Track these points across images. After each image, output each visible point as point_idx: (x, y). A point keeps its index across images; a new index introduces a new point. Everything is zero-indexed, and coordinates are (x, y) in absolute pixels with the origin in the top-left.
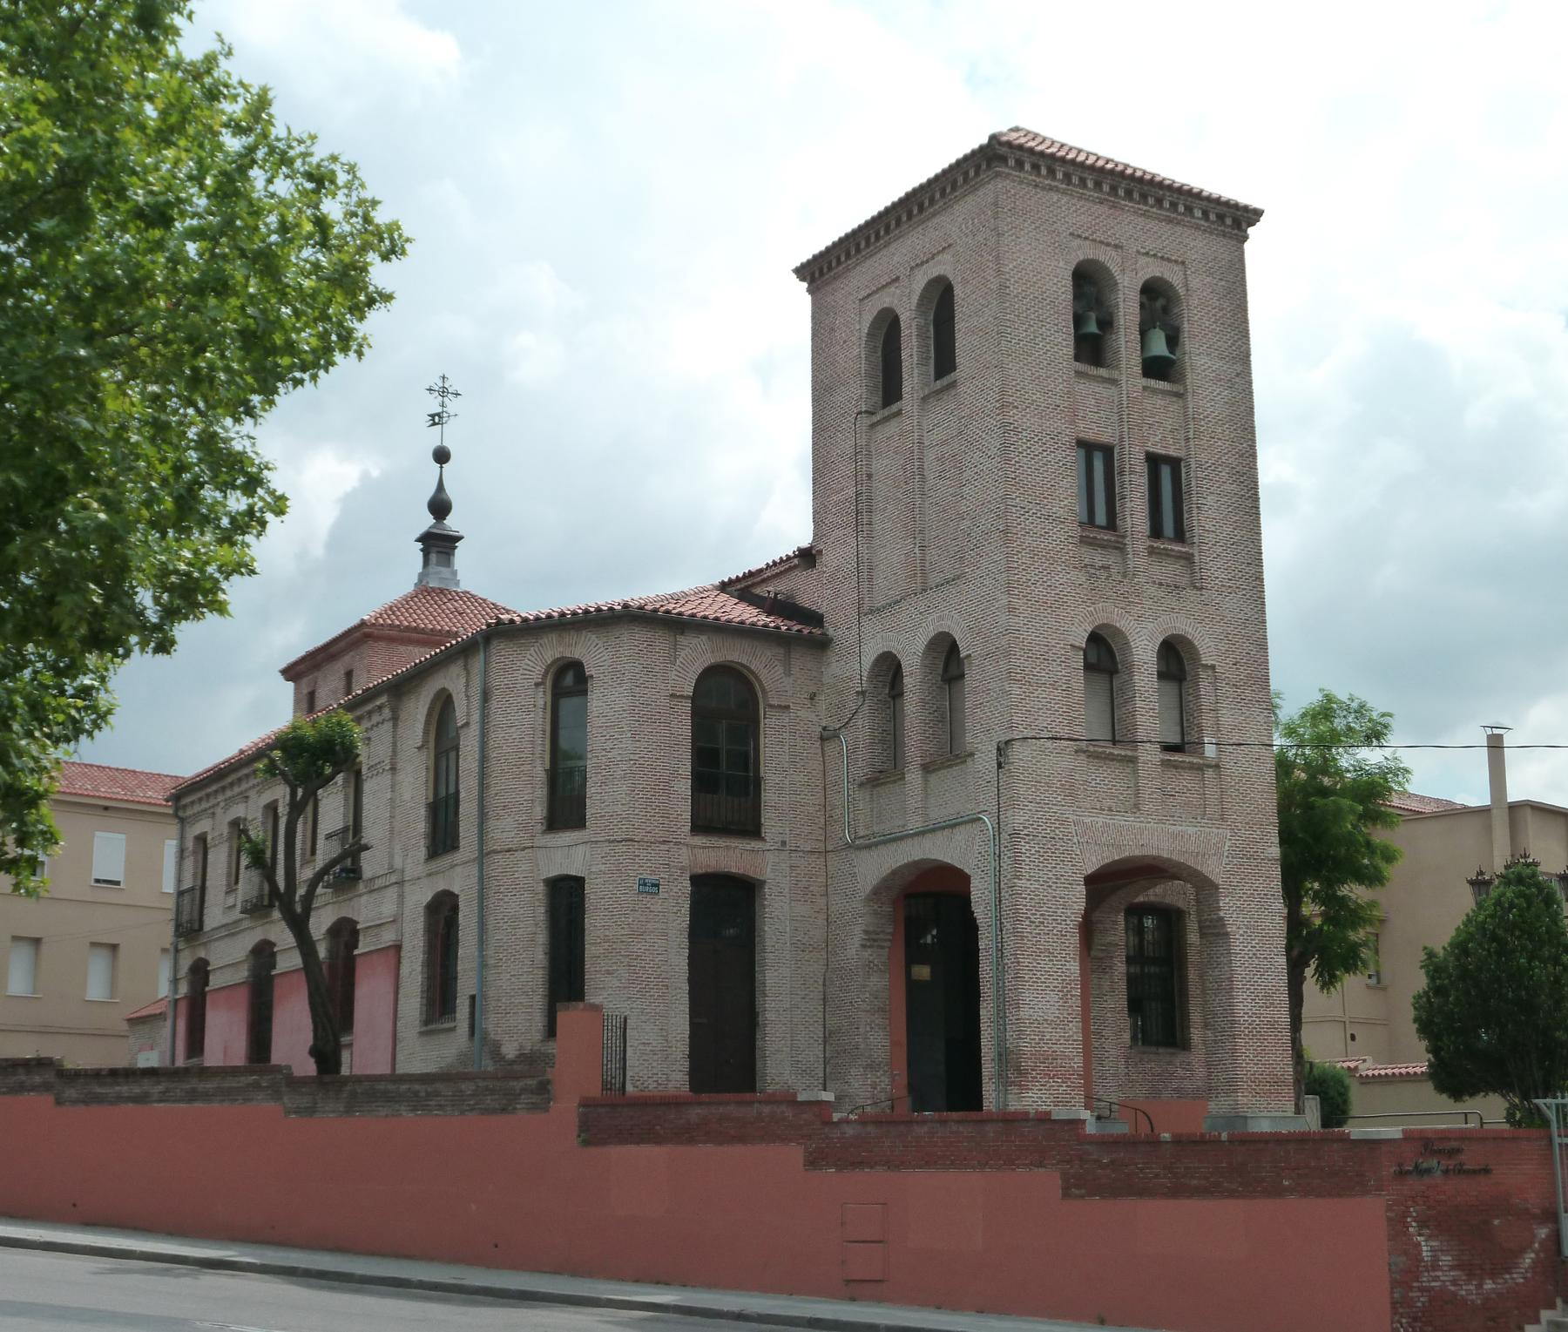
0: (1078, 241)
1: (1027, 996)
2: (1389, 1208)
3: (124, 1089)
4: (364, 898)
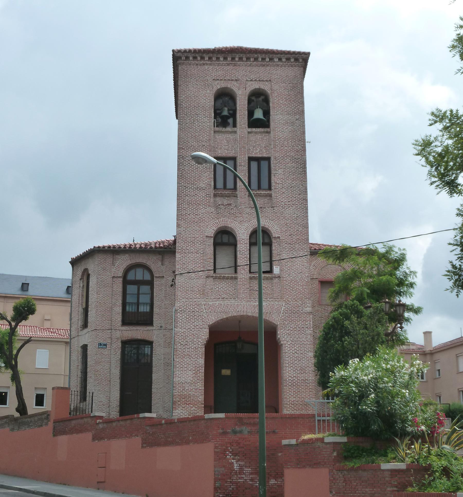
0: (218, 81)
1: (177, 373)
2: (216, 447)
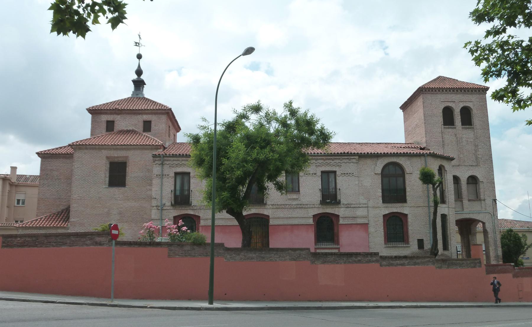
3: (398, 262)
4: (342, 209)
